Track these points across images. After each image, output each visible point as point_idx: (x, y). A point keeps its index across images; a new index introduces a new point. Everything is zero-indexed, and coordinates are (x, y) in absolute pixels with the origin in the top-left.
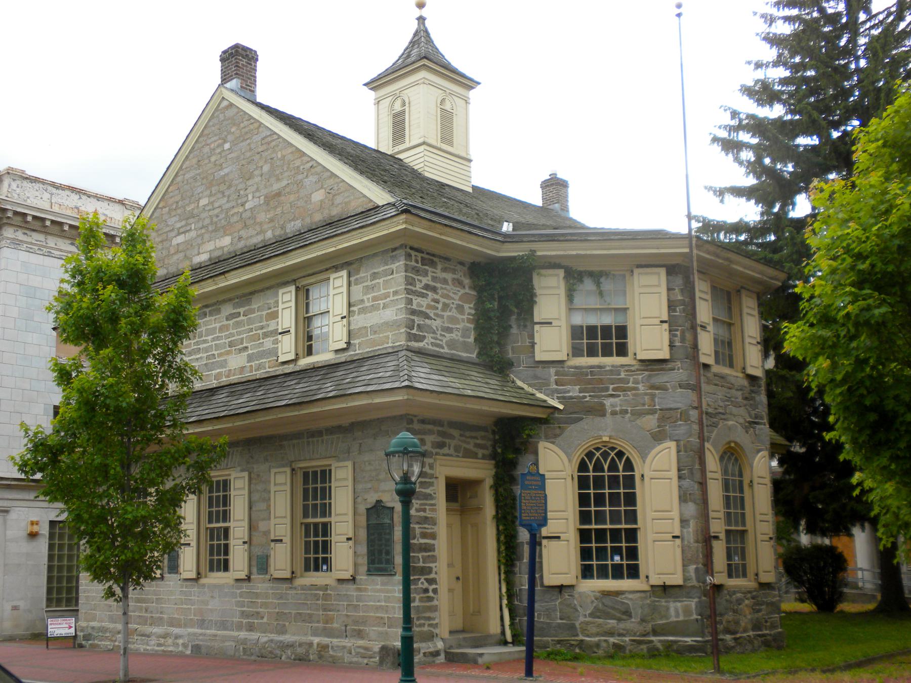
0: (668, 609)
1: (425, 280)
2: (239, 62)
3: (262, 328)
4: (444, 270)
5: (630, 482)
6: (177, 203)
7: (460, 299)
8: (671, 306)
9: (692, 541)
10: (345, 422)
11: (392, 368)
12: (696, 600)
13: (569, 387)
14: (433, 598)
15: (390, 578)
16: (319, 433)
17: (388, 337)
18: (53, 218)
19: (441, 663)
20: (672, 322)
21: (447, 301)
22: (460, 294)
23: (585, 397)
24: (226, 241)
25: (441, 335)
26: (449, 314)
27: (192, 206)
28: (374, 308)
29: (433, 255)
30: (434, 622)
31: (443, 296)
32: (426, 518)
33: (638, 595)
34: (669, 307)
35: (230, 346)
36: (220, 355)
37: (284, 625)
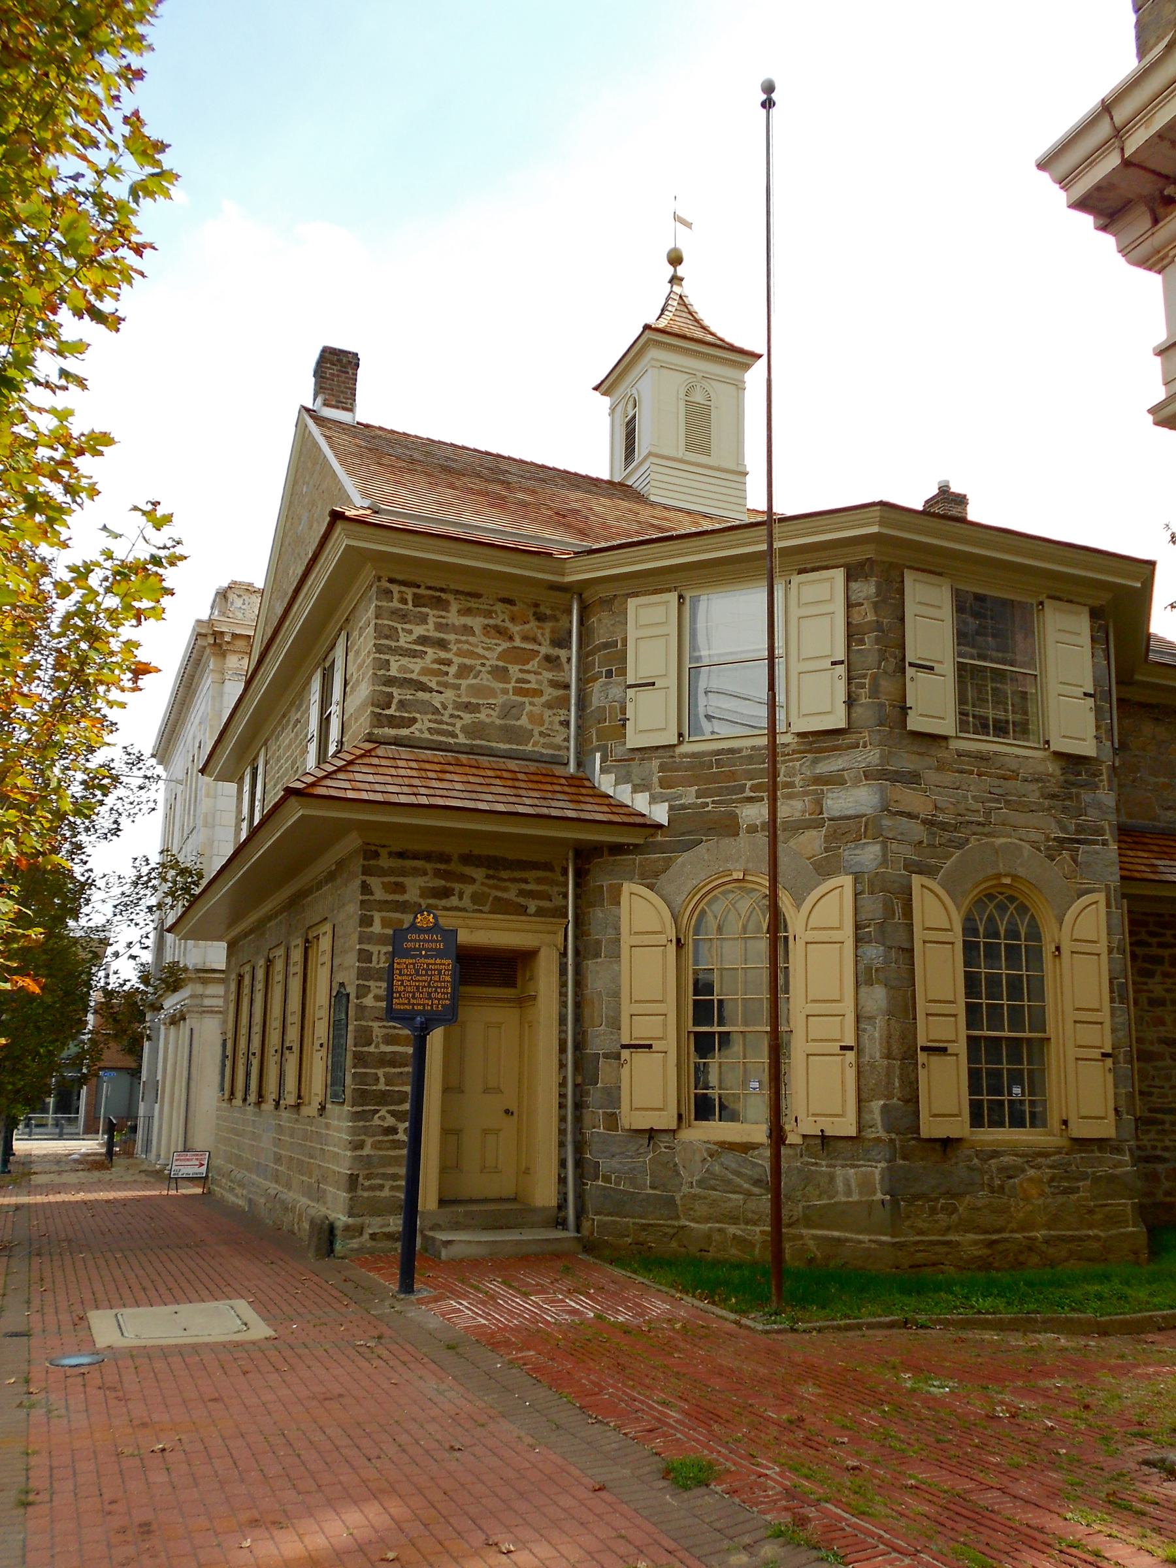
0: (832, 1178)
2: (337, 371)
4: (467, 612)
8: (853, 634)
9: (878, 1055)
12: (883, 1165)
21: (467, 661)
22: (500, 649)
23: (707, 804)
25: (452, 716)
31: (460, 653)
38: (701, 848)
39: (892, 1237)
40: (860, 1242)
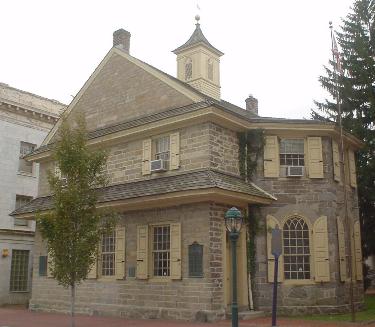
0: (323, 292)
1: (218, 138)
2: (121, 37)
3: (133, 159)
4: (225, 134)
5: (306, 234)
6: (90, 99)
7: (231, 148)
8: (324, 155)
9: (333, 261)
10: (178, 204)
11: (205, 179)
12: (335, 288)
13: (280, 190)
14: (221, 289)
15: (201, 279)
16: (163, 209)
17: (200, 164)
18: (20, 107)
19: (224, 320)
20: (324, 162)
23: (287, 195)
24: (115, 118)
26: (227, 154)
27: (97, 101)
28: (193, 150)
29: (221, 127)
30: (221, 300)
32: (218, 250)
33: (310, 286)
34: (323, 155)
35: (116, 167)
36: (110, 171)
37: (144, 302)
38: (285, 207)
39: (338, 305)
40: (331, 307)
